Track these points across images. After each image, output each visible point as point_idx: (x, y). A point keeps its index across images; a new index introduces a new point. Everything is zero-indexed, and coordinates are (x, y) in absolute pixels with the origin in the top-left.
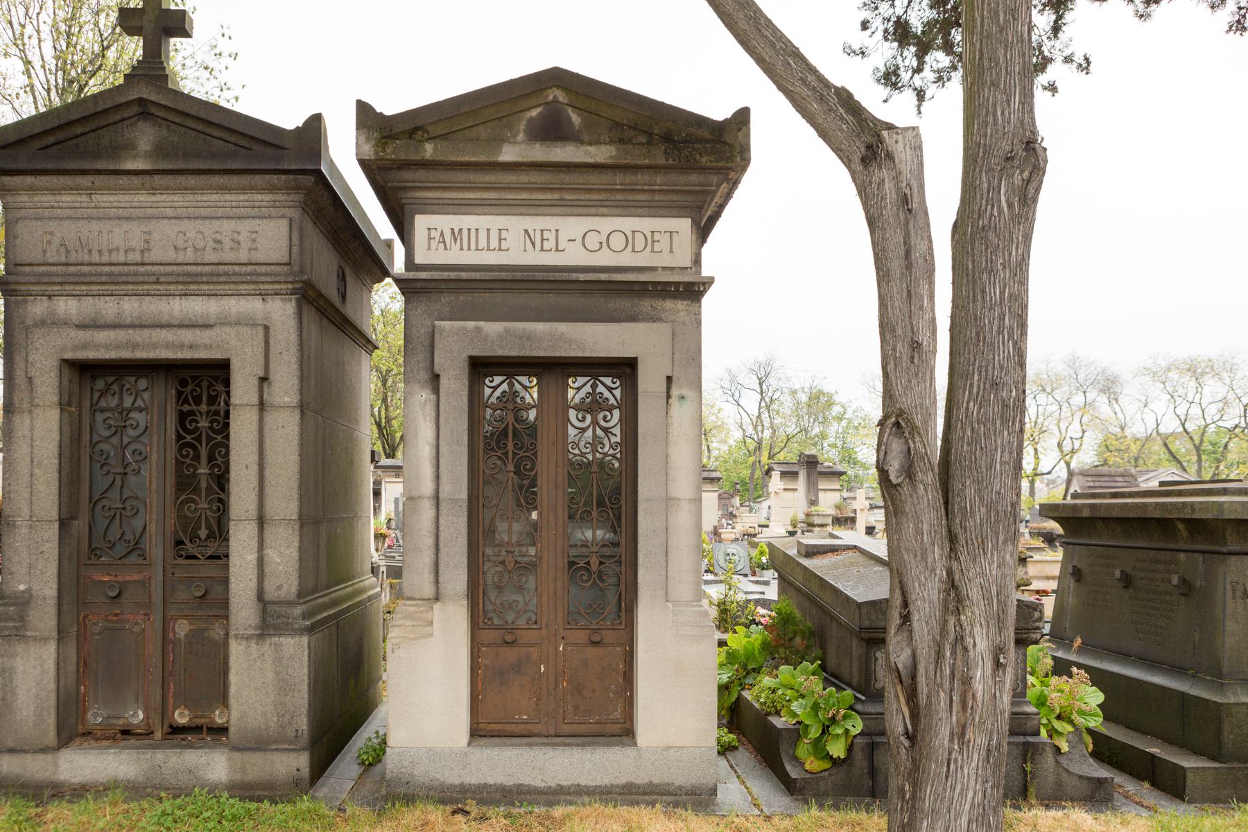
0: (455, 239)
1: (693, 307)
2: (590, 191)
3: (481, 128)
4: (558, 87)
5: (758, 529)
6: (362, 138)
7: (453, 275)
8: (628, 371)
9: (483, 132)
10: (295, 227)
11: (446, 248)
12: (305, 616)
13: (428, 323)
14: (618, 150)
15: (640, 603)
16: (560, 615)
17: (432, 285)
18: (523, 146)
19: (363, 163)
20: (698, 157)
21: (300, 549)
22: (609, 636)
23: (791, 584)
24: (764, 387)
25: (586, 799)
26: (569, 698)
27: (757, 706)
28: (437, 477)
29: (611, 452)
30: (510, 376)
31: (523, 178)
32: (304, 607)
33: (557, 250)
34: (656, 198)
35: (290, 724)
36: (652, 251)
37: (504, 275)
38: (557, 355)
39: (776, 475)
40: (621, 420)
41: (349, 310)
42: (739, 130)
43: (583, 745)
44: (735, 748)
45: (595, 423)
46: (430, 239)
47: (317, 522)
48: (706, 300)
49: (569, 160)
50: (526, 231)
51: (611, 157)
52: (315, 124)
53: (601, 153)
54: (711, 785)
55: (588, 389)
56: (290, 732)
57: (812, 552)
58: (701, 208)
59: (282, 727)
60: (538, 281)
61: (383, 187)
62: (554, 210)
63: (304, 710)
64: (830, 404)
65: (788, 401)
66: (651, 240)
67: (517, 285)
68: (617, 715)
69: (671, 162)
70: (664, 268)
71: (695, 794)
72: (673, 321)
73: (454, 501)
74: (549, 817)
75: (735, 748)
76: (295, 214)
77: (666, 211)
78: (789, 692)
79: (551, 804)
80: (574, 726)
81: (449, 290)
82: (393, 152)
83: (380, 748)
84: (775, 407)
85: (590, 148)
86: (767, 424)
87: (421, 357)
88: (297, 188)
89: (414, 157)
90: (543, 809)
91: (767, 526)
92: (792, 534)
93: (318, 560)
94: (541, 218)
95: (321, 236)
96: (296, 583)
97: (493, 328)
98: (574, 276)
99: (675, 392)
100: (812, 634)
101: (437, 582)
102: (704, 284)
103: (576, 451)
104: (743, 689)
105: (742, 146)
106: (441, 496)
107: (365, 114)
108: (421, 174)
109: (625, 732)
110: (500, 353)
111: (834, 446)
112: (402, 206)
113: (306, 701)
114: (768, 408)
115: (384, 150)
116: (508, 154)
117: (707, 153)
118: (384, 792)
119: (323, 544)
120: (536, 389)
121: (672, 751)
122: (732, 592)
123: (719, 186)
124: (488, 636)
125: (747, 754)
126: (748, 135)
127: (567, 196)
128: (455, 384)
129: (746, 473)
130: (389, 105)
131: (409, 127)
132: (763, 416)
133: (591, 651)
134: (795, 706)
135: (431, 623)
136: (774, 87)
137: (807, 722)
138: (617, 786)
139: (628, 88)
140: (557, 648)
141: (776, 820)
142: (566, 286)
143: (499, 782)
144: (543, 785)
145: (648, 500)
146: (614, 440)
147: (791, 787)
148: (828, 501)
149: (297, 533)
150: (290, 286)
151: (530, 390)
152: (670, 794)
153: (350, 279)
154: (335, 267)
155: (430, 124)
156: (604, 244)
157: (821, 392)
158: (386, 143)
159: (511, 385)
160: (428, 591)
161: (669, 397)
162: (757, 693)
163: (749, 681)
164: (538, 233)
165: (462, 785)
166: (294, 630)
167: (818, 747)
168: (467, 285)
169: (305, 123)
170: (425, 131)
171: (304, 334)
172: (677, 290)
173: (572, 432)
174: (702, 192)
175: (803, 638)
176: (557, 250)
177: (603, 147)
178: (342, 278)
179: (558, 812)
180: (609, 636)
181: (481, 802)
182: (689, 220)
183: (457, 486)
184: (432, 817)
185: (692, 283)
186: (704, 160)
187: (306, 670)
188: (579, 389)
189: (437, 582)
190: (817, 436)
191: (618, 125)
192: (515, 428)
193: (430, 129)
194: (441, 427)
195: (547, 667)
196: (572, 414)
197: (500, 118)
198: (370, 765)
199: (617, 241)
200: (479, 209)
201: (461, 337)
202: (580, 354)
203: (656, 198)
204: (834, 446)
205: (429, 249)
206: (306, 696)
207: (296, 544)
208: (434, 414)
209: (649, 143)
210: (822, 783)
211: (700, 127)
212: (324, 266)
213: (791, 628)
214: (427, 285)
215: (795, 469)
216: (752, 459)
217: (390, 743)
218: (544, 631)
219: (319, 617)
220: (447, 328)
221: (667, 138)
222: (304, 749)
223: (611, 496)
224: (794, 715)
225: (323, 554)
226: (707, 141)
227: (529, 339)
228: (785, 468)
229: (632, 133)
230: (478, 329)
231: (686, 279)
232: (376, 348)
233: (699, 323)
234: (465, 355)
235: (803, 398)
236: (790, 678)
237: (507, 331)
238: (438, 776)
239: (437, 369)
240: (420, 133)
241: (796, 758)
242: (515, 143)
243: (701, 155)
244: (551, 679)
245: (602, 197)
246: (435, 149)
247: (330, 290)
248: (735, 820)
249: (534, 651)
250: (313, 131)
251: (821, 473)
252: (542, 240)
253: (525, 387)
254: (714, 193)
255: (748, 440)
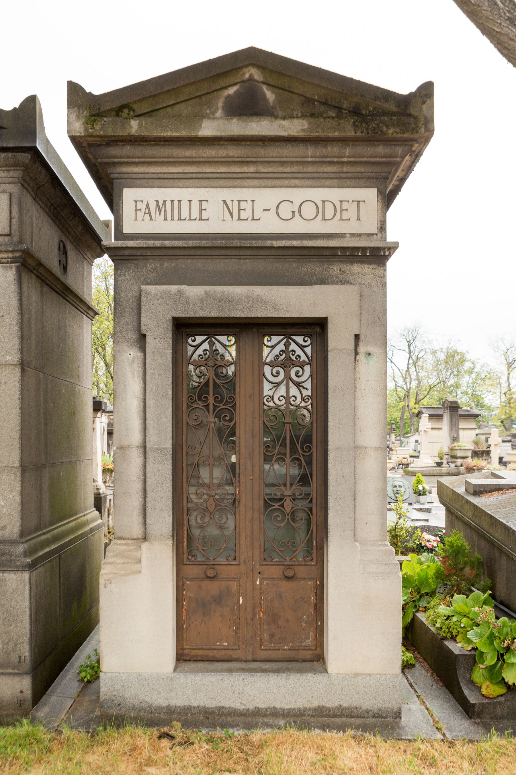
0: (160, 211)
1: (379, 271)
2: (283, 163)
3: (182, 106)
4: (254, 65)
5: (410, 460)
6: (73, 116)
7: (158, 243)
8: (318, 330)
9: (184, 109)
10: (14, 201)
11: (151, 219)
12: (26, 554)
13: (135, 287)
14: (310, 123)
15: (330, 543)
16: (257, 552)
17: (139, 253)
18: (221, 122)
19: (74, 139)
20: (385, 129)
21: (22, 494)
22: (301, 571)
23: (458, 518)
24: (412, 348)
25: (282, 722)
26: (266, 627)
27: (433, 629)
28: (145, 428)
29: (303, 404)
30: (210, 336)
31: (222, 152)
32: (26, 546)
33: (253, 219)
34: (345, 169)
35: (14, 651)
36: (341, 219)
37: (204, 243)
38: (254, 315)
39: (425, 418)
40: (311, 375)
41: (71, 280)
42: (424, 103)
43: (277, 671)
44: (413, 666)
45: (288, 378)
46: (136, 210)
47: (39, 468)
48: (390, 263)
49: (264, 133)
50: (225, 202)
51: (303, 130)
52: (30, 104)
53: (294, 127)
54: (396, 709)
55: (281, 347)
56: (14, 658)
57: (479, 491)
58: (386, 178)
59: (7, 653)
60: (235, 248)
61: (95, 165)
62: (250, 182)
63: (26, 639)
64: (463, 361)
65: (430, 358)
66: (340, 209)
67: (217, 252)
68: (309, 642)
69: (359, 134)
70: (351, 235)
71: (381, 717)
72: (360, 284)
73: (160, 450)
74: (248, 742)
75: (413, 666)
76: (15, 189)
77: (353, 182)
78: (464, 620)
79: (249, 727)
80: (270, 652)
81: (154, 257)
82: (101, 129)
83: (95, 670)
84: (420, 363)
85: (284, 123)
86: (414, 376)
87: (129, 319)
88: (16, 165)
89: (120, 133)
90: (242, 732)
91: (418, 457)
92: (439, 464)
93: (41, 502)
94: (238, 190)
95: (41, 211)
96: (18, 524)
97: (195, 291)
98: (269, 243)
99: (362, 349)
100: (481, 564)
101: (145, 523)
102: (389, 249)
103: (271, 404)
104: (418, 611)
105: (426, 118)
106: (148, 445)
107: (75, 93)
108: (128, 150)
109: (313, 658)
110: (201, 314)
111: (465, 393)
112: (111, 181)
113: (28, 630)
114: (415, 364)
115: (93, 128)
116: (208, 129)
117: (393, 125)
118: (98, 712)
119: (46, 486)
120: (234, 347)
121: (360, 677)
122: (401, 521)
123: (403, 157)
124: (192, 571)
125: (423, 672)
126: (431, 107)
127: (262, 169)
128: (160, 342)
129: (397, 415)
130: (98, 86)
131: (116, 104)
132: (411, 371)
133: (285, 585)
134: (470, 635)
135: (139, 561)
136: (478, 32)
137: (482, 650)
138: (310, 709)
139: (319, 66)
140: (254, 582)
141: (459, 746)
142: (261, 252)
143: (202, 704)
144: (242, 707)
145: (337, 448)
146: (305, 393)
147: (468, 710)
148: (467, 438)
149: (19, 479)
150: (11, 255)
151: (228, 347)
152: (358, 716)
153: (71, 252)
154: (56, 241)
155: (135, 102)
156: (297, 214)
157: (455, 352)
158: (95, 121)
159: (211, 344)
160: (137, 531)
161: (356, 353)
162: (437, 614)
163: (423, 604)
164: (236, 204)
165: (168, 707)
166: (16, 567)
167: (494, 674)
168: (171, 252)
169: (21, 105)
170: (131, 109)
171: (25, 299)
172: (364, 255)
173: (267, 386)
174: (388, 163)
175: (472, 567)
176: (253, 219)
177: (296, 121)
178: (63, 251)
179: (257, 736)
180: (301, 571)
181: (186, 724)
182: (376, 190)
183: (162, 436)
184: (139, 742)
185: (378, 249)
186: (391, 131)
187: (27, 603)
188: (273, 347)
189: (145, 523)
190: (452, 386)
191: (309, 101)
192: (215, 383)
193: (135, 107)
194: (148, 382)
195: (245, 599)
196: (267, 370)
197: (200, 96)
198: (89, 682)
199: (309, 211)
200: (181, 183)
201: (166, 300)
202: (274, 315)
203: (345, 169)
204: (465, 393)
205: (136, 219)
206: (28, 626)
207: (19, 488)
208: (141, 370)
209: (339, 117)
210: (499, 708)
211: (387, 101)
212: (45, 240)
213: (463, 560)
214: (135, 252)
215: (440, 412)
216: (402, 404)
217: (105, 667)
218: (243, 567)
219: (41, 553)
220: (153, 292)
221: (356, 112)
222: (26, 673)
223: (304, 443)
224: (469, 641)
225: (46, 496)
226: (393, 114)
227: (227, 301)
228: (432, 412)
229: (322, 108)
230: (181, 293)
231: (372, 245)
232: (96, 313)
233: (384, 285)
234: (169, 317)
235: (442, 356)
236: (464, 607)
237: (207, 294)
238: (147, 699)
239: (143, 330)
240: (126, 111)
241: (472, 682)
242: (214, 118)
243: (387, 127)
244: (249, 609)
245: (295, 169)
246: (140, 125)
247: (52, 262)
248: (421, 746)
249: (233, 585)
250: (29, 110)
251: (461, 416)
252: (240, 210)
253: (225, 346)
254: (399, 164)
255: (399, 389)
